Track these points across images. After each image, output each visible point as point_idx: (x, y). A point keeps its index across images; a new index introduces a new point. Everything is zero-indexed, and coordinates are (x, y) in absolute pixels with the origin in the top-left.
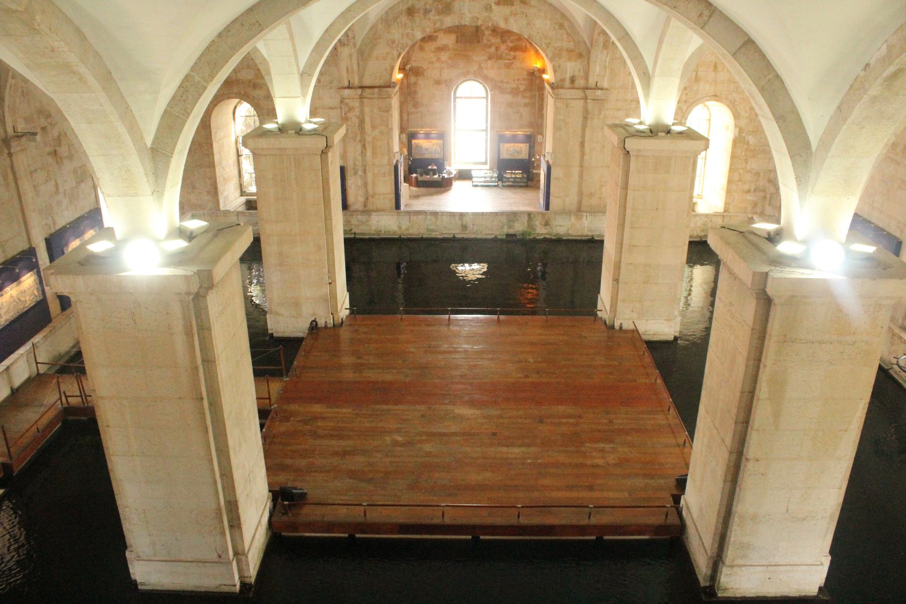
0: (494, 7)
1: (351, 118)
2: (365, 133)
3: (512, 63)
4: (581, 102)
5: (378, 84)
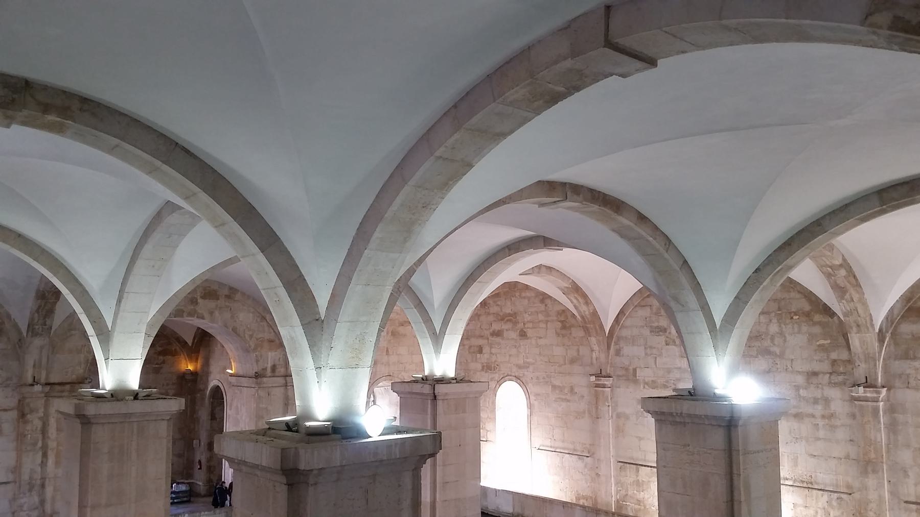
0: (200, 301)
1: (32, 421)
2: (48, 437)
3: (161, 368)
4: (282, 389)
5: (69, 381)
